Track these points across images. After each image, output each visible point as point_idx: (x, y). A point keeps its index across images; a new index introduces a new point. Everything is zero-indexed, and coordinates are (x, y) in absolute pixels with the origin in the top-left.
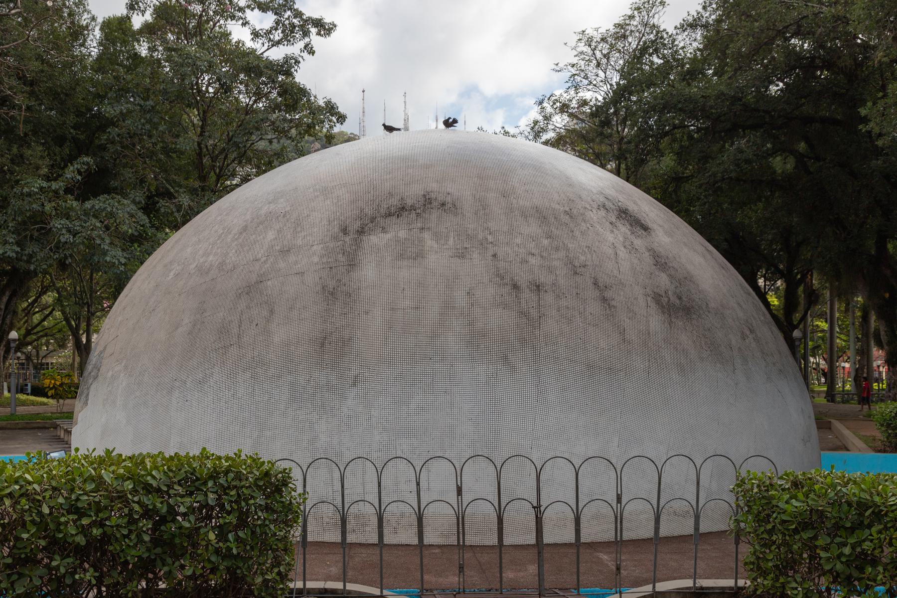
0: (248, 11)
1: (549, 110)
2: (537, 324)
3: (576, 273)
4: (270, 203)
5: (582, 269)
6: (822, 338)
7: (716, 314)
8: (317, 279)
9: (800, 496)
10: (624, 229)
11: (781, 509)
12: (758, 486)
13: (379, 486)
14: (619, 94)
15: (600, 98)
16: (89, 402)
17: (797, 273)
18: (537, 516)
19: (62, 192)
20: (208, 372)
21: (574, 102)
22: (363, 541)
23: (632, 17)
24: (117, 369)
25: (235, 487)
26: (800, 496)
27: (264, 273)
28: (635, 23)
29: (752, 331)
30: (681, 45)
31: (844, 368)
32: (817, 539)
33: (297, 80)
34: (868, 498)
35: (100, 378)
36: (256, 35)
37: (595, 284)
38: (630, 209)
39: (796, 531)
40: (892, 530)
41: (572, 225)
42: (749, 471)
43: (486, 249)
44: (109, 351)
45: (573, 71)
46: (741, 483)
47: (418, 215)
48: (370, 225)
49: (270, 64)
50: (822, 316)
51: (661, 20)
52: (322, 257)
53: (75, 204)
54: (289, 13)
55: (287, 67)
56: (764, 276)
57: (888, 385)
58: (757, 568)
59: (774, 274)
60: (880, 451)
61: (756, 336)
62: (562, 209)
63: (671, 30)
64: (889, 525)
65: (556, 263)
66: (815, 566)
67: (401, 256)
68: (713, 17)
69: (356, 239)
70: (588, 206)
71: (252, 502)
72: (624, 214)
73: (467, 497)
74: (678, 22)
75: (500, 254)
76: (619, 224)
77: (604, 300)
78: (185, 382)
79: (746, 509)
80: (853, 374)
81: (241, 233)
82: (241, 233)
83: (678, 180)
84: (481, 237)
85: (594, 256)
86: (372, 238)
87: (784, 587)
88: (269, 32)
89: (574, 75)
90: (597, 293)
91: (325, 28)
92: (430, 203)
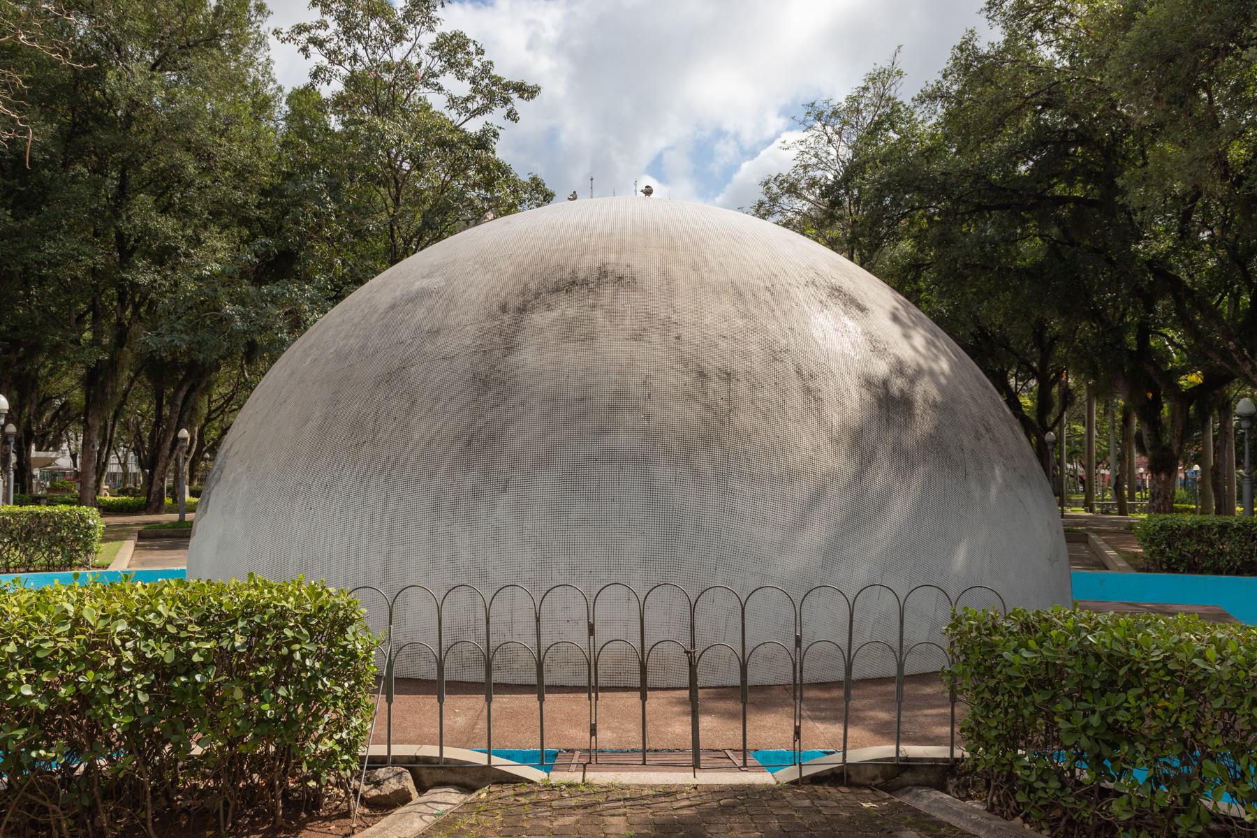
1: (775, 189)
2: (726, 419)
3: (775, 359)
6: (1080, 443)
7: (945, 409)
8: (468, 365)
9: (1032, 643)
10: (837, 309)
12: (978, 628)
13: (488, 622)
14: (852, 171)
15: (831, 177)
18: (690, 664)
20: (336, 474)
22: (509, 681)
23: (866, 89)
24: (239, 470)
26: (1032, 643)
29: (988, 430)
30: (920, 119)
32: (1055, 703)
34: (1123, 650)
37: (799, 372)
38: (845, 288)
39: (1026, 691)
40: (1156, 696)
41: (773, 303)
42: (966, 608)
43: (669, 330)
44: (235, 449)
46: (956, 622)
47: (590, 290)
48: (534, 302)
49: (466, 139)
50: (1080, 418)
52: (475, 338)
53: (251, 289)
54: (487, 81)
55: (482, 142)
56: (1016, 375)
57: (1152, 494)
58: (975, 734)
59: (1027, 371)
60: (1142, 570)
62: (762, 284)
63: (908, 102)
64: (1152, 689)
65: (753, 348)
66: (1052, 737)
67: (567, 338)
68: (955, 87)
71: (297, 646)
72: (836, 292)
73: (601, 636)
74: (916, 93)
75: (685, 336)
76: (830, 303)
78: (310, 487)
79: (962, 658)
80: (1113, 483)
81: (387, 312)
82: (387, 312)
83: (916, 267)
85: (798, 339)
86: (534, 316)
87: (1011, 764)
90: (801, 382)
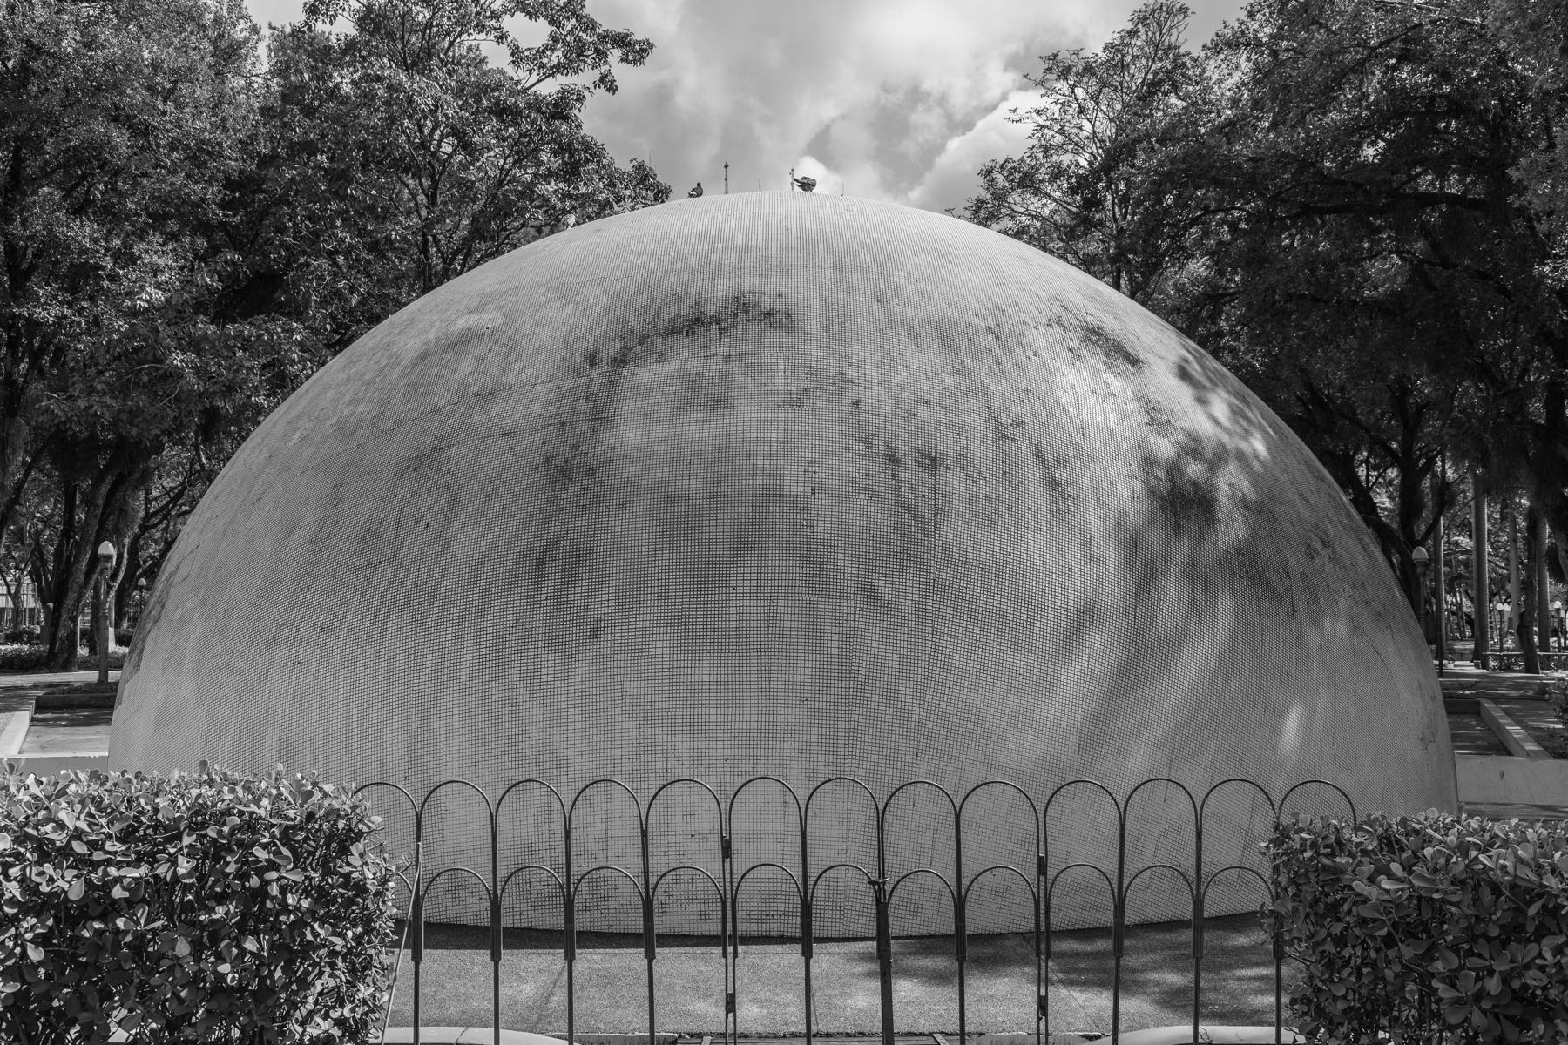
0: (506, 17)
2: (930, 527)
3: (1003, 436)
4: (470, 312)
5: (1015, 430)
6: (1466, 564)
8: (538, 444)
10: (1096, 361)
11: (1358, 895)
15: (1084, 163)
16: (142, 664)
17: (1420, 457)
18: (878, 900)
19: (189, 310)
21: (1043, 170)
22: (604, 929)
23: (1133, 33)
24: (190, 604)
25: (240, 844)
27: (447, 433)
28: (1139, 43)
30: (1215, 77)
31: (1501, 612)
33: (586, 129)
34: (1533, 877)
35: (163, 620)
36: (517, 56)
37: (1039, 455)
38: (1107, 328)
39: (1389, 941)
43: (842, 391)
44: (182, 572)
45: (1041, 120)
46: (1281, 835)
47: (723, 331)
48: (637, 349)
49: (536, 104)
50: (1464, 527)
51: (1181, 39)
56: (1367, 461)
59: (1384, 457)
61: (1334, 552)
62: (982, 324)
65: (970, 419)
67: (689, 404)
68: (1268, 30)
69: (610, 374)
70: (1029, 321)
71: (273, 875)
72: (1094, 335)
73: (740, 863)
75: (867, 402)
76: (1084, 352)
77: (1054, 484)
78: (297, 629)
80: (1516, 623)
81: (415, 365)
82: (415, 365)
83: (1214, 298)
84: (833, 371)
85: (1038, 407)
86: (638, 370)
88: (542, 52)
89: (1042, 126)
90: (1042, 472)
91: (636, 51)
92: (746, 312)
